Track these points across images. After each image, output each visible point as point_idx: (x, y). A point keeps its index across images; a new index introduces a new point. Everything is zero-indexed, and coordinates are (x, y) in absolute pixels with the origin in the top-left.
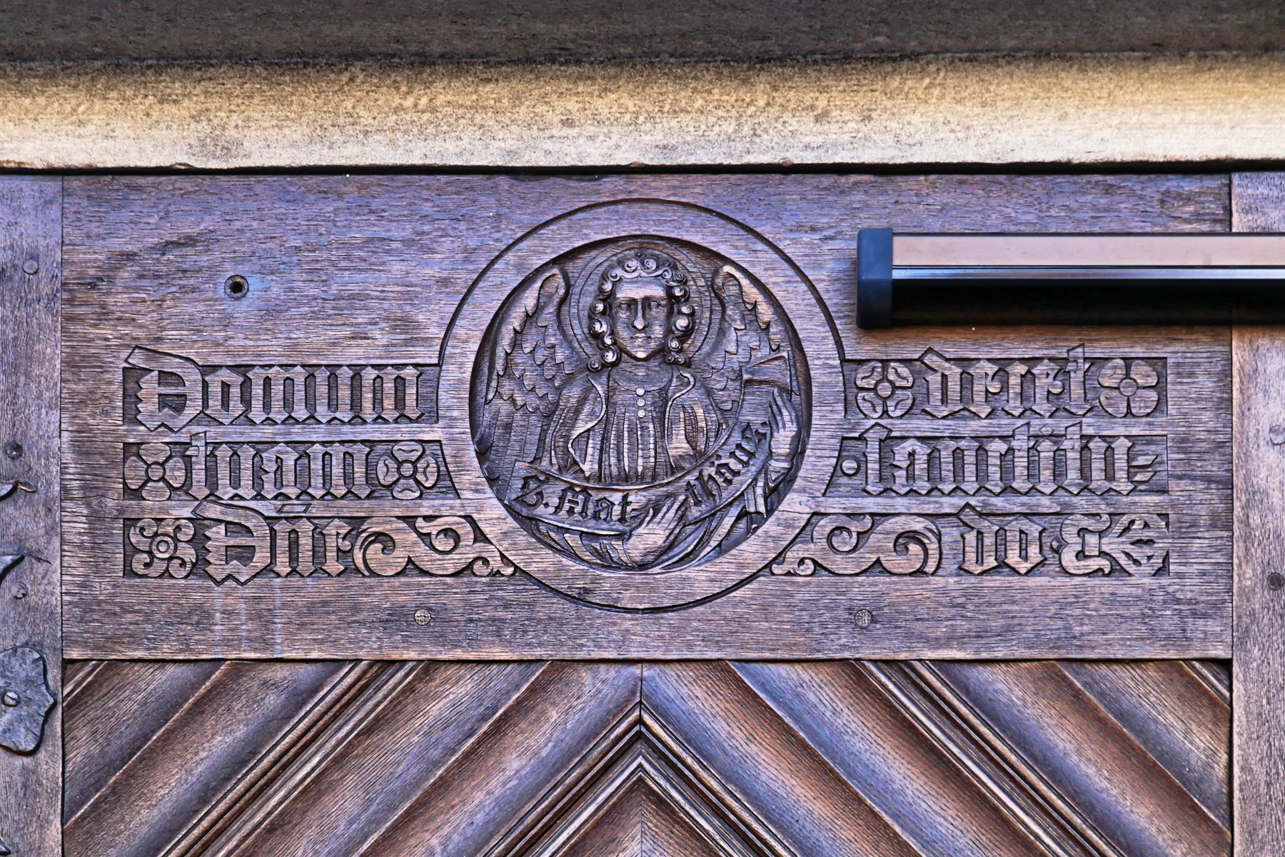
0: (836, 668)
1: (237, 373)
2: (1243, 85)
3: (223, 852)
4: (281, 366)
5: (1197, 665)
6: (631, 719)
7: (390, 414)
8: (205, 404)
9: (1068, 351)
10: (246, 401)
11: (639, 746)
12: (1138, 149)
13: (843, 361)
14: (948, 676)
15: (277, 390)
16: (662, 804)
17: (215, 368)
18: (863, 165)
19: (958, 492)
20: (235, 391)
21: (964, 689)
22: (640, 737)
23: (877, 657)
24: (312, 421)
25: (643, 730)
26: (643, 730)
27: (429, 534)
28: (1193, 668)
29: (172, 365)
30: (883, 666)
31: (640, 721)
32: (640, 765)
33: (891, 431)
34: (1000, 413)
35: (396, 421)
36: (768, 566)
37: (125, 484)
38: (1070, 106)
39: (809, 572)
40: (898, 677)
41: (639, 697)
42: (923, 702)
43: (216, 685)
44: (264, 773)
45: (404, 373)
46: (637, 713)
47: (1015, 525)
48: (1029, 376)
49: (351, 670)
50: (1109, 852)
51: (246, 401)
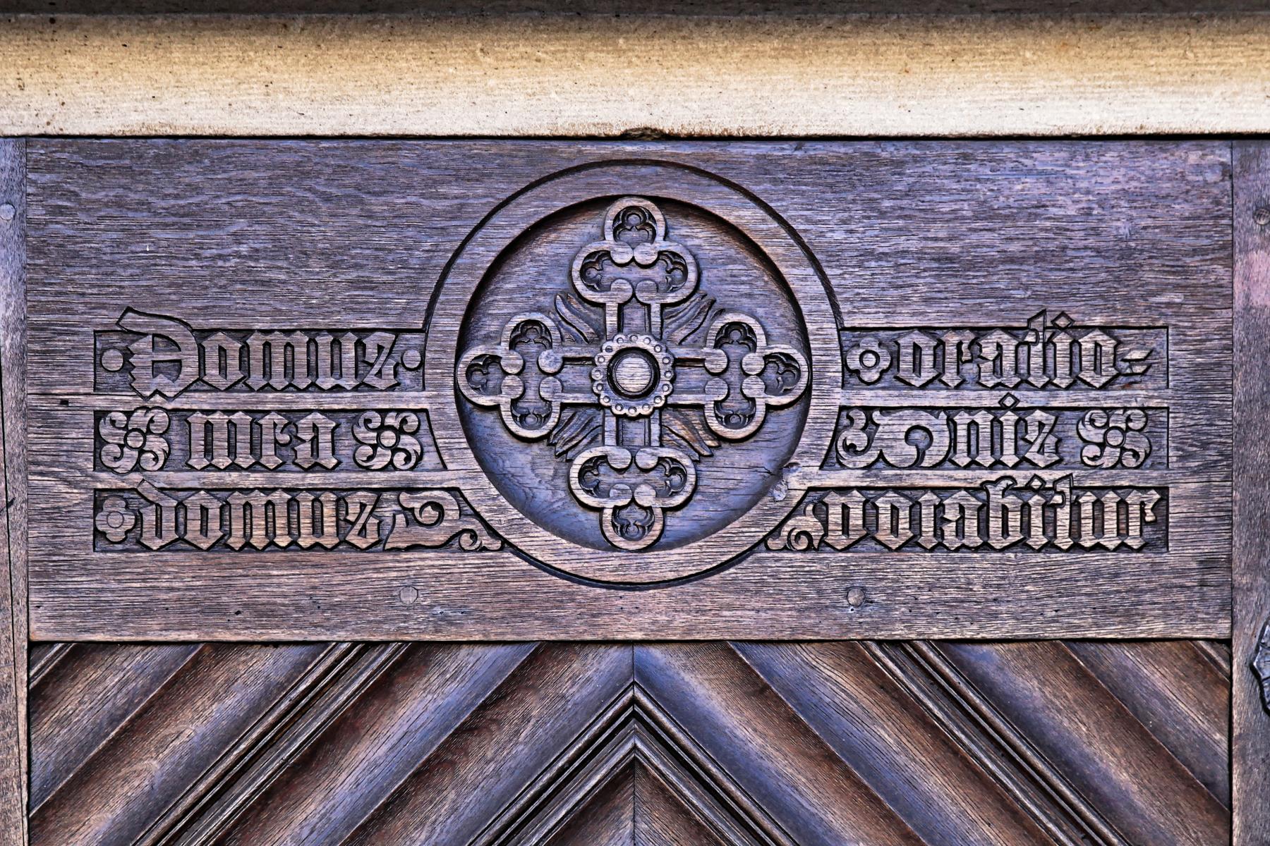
0: (841, 647)
1: (234, 338)
2: (1143, 41)
3: (149, 841)
5: (874, 647)
6: (625, 699)
7: (278, 381)
11: (634, 725)
12: (164, 118)
13: (841, 329)
14: (949, 655)
15: (278, 356)
19: (317, 468)
21: (960, 666)
22: (634, 715)
24: (200, 386)
25: (637, 709)
26: (637, 709)
27: (412, 510)
28: (867, 648)
29: (171, 329)
30: (886, 647)
35: (355, 389)
36: (764, 540)
38: (708, 71)
39: (804, 547)
41: (641, 675)
42: (940, 686)
44: (241, 758)
46: (630, 694)
47: (1133, 498)
49: (61, 649)
50: (783, 839)
51: (245, 366)
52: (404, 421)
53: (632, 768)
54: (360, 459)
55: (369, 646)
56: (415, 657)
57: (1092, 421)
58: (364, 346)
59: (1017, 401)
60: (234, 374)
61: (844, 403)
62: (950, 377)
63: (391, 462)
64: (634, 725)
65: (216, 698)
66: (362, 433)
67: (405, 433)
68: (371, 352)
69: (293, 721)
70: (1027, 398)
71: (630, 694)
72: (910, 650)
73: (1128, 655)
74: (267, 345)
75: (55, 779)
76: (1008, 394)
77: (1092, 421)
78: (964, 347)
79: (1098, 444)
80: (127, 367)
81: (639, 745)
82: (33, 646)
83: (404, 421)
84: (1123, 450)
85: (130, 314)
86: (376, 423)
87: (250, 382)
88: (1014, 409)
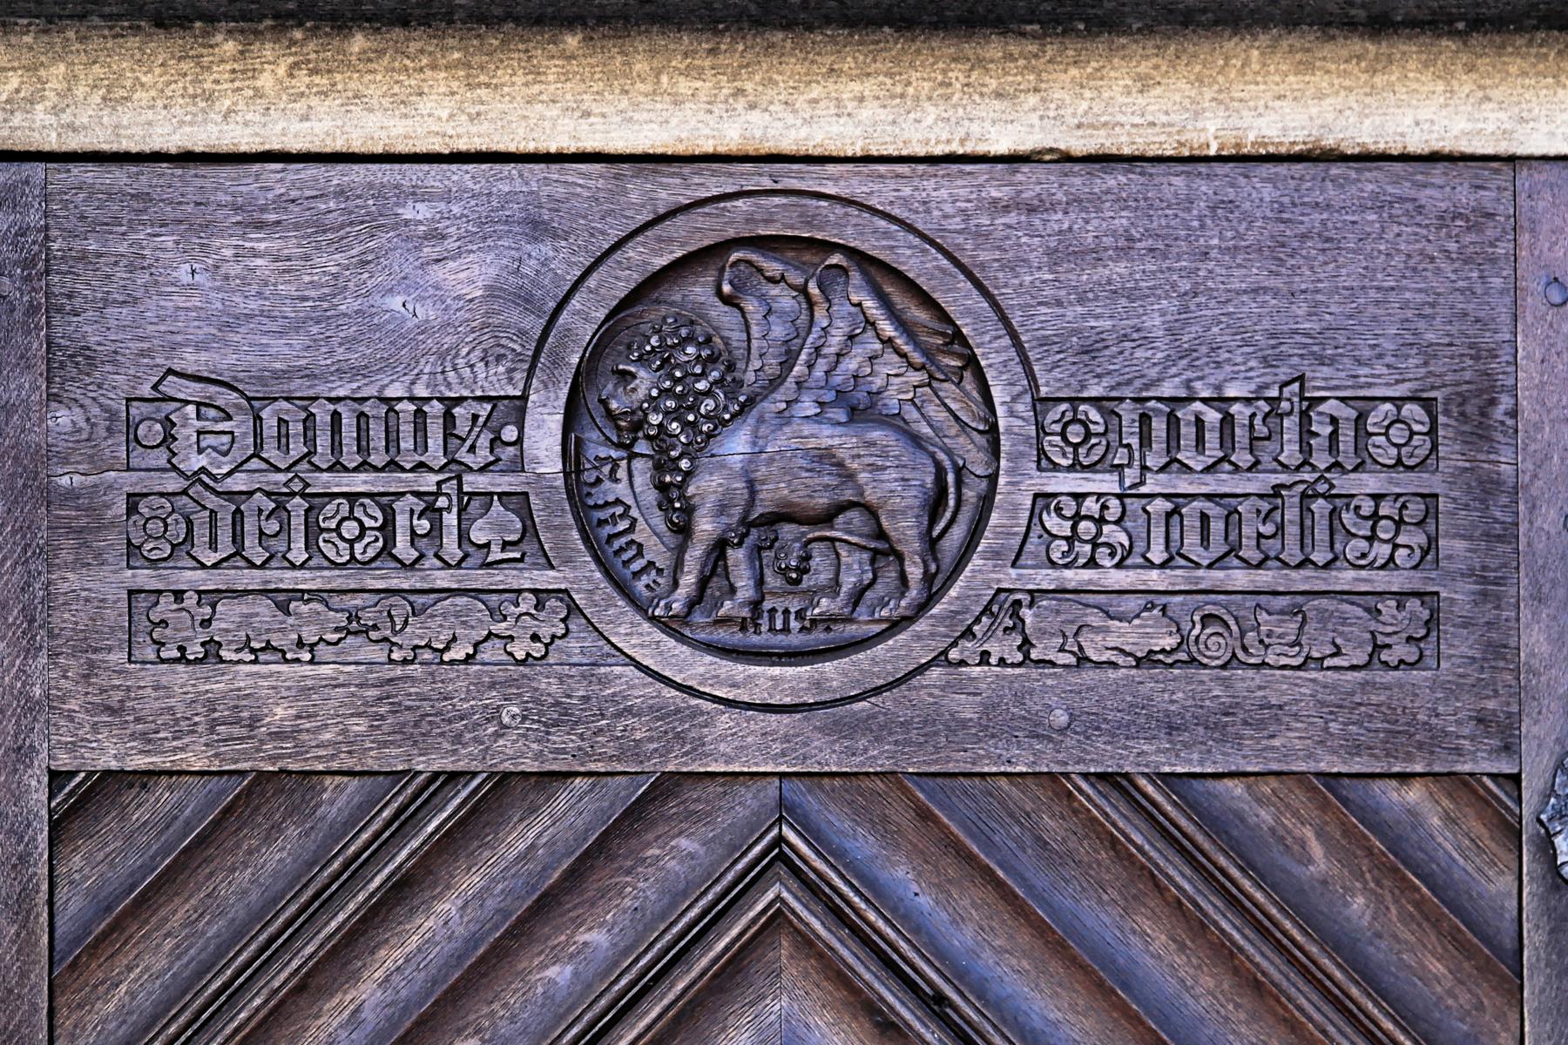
4: (1342, 399)
7: (351, 458)
8: (259, 445)
9: (1281, 388)
10: (310, 440)
16: (807, 943)
17: (459, 400)
18: (416, 155)
20: (296, 428)
21: (1191, 806)
22: (780, 857)
23: (1495, 771)
26: (786, 849)
30: (1501, 780)
31: (781, 839)
32: (778, 898)
33: (307, 485)
34: (1369, 464)
37: (129, 540)
40: (1114, 795)
43: (260, 795)
45: (366, 408)
46: (775, 831)
48: (392, 414)
52: (1104, 507)
53: (777, 919)
54: (1056, 556)
55: (453, 777)
56: (505, 792)
57: (1058, 510)
58: (261, 419)
59: (307, 485)
60: (1213, 451)
61: (1036, 489)
62: (1243, 458)
63: (1391, 558)
64: (782, 870)
65: (1448, 819)
66: (1052, 522)
67: (1108, 522)
68: (462, 428)
69: (1182, 851)
70: (1343, 483)
71: (775, 831)
72: (1125, 783)
73: (1236, 788)
74: (336, 416)
75: (77, 941)
76: (1322, 477)
77: (1058, 510)
78: (1258, 421)
79: (1066, 538)
80: (169, 438)
81: (785, 894)
82: (53, 775)
83: (1104, 507)
84: (1095, 546)
85: (170, 378)
86: (1367, 509)
87: (315, 459)
88: (1327, 497)
